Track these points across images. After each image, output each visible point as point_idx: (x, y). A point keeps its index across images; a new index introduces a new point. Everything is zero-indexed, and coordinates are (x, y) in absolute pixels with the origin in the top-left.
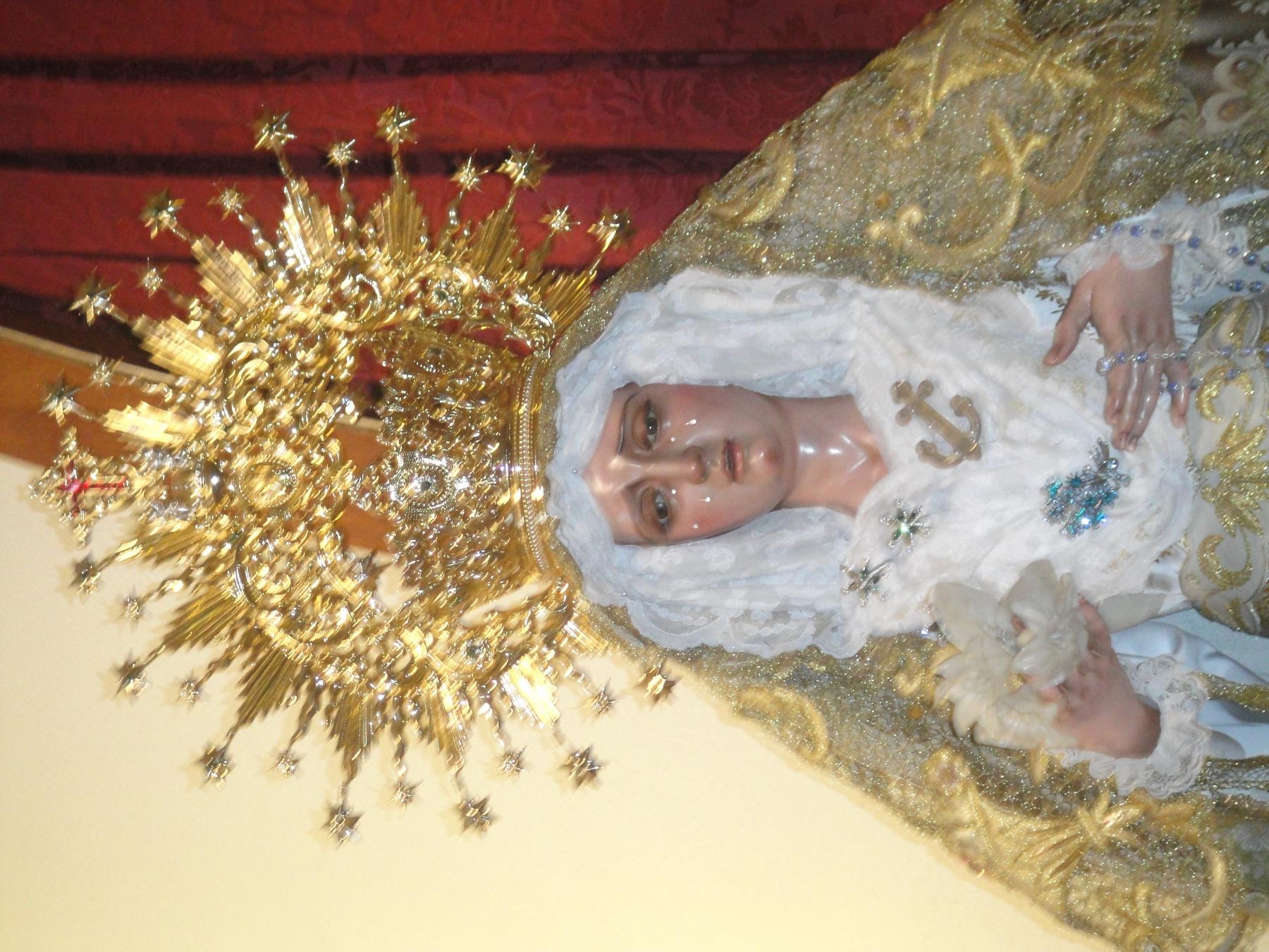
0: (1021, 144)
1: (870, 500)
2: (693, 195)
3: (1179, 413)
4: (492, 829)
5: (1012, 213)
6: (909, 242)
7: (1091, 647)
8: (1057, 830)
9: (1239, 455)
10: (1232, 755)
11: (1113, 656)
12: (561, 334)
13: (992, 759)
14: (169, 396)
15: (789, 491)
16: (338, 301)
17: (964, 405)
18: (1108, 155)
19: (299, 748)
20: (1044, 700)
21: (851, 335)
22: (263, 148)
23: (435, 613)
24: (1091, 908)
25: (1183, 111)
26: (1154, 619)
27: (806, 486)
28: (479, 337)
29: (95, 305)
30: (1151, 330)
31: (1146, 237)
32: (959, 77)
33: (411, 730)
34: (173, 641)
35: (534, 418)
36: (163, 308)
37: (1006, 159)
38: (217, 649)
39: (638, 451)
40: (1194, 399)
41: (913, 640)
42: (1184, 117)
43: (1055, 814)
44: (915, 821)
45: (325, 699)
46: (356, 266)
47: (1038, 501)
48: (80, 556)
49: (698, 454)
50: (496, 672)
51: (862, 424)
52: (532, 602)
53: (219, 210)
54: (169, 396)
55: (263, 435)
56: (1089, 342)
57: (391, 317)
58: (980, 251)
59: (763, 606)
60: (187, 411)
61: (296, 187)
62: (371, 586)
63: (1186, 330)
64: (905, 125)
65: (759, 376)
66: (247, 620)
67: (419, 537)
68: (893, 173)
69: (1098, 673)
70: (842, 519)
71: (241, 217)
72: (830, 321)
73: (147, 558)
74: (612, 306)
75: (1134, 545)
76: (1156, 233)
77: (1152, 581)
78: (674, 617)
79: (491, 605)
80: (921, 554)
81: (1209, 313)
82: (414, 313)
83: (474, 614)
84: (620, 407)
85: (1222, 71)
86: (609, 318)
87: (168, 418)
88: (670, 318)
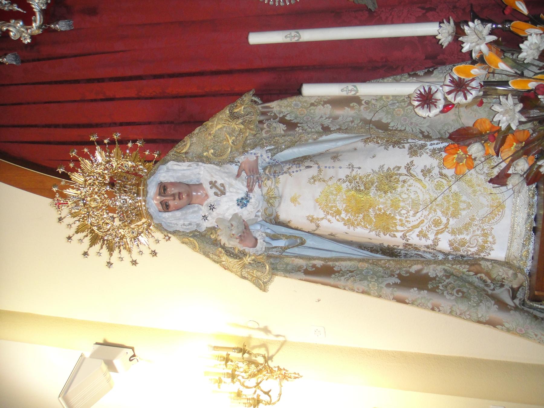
0: (231, 138)
1: (206, 203)
2: (172, 147)
3: (260, 187)
4: (137, 265)
5: (230, 150)
6: (212, 155)
7: (245, 228)
8: (240, 261)
9: (271, 193)
10: (271, 246)
11: (249, 230)
12: (148, 173)
13: (228, 249)
14: (75, 187)
15: (191, 201)
16: (106, 169)
17: (222, 185)
18: (246, 140)
19: (101, 251)
20: (237, 239)
21: (202, 173)
22: (92, 140)
23: (125, 226)
24: (246, 275)
25: (259, 132)
26: (257, 223)
27: (194, 201)
28: (133, 174)
29: (61, 170)
30: (255, 171)
31: (253, 155)
32: (219, 126)
33: (122, 247)
34: (77, 232)
35: (143, 189)
36: (74, 170)
37: (228, 141)
38: (85, 234)
39: (163, 195)
40: (263, 183)
41: (214, 228)
42: (259, 133)
43: (240, 258)
44: (215, 261)
45: (105, 242)
46: (108, 162)
47: (235, 203)
48: (59, 216)
49: (173, 195)
50: (137, 236)
51: (203, 189)
52: (143, 223)
53: (84, 151)
54: (75, 187)
55: (93, 193)
56: (244, 174)
57: (116, 171)
58: (224, 157)
59: (186, 223)
60: (78, 189)
61: (98, 147)
62: (113, 221)
63: (261, 171)
64: (210, 134)
65: (184, 180)
66: (90, 228)
67: (122, 211)
68: (209, 143)
69: (247, 233)
70: (200, 206)
71: (88, 153)
72: (198, 170)
73: (72, 217)
74: (158, 168)
75: (253, 210)
76: (255, 154)
77: (256, 216)
78: (171, 225)
79: (136, 224)
80: (215, 213)
81: (265, 168)
82: (120, 170)
83: (132, 226)
84: (159, 186)
85: (265, 126)
86: (157, 170)
87: (75, 191)
88: (168, 170)
